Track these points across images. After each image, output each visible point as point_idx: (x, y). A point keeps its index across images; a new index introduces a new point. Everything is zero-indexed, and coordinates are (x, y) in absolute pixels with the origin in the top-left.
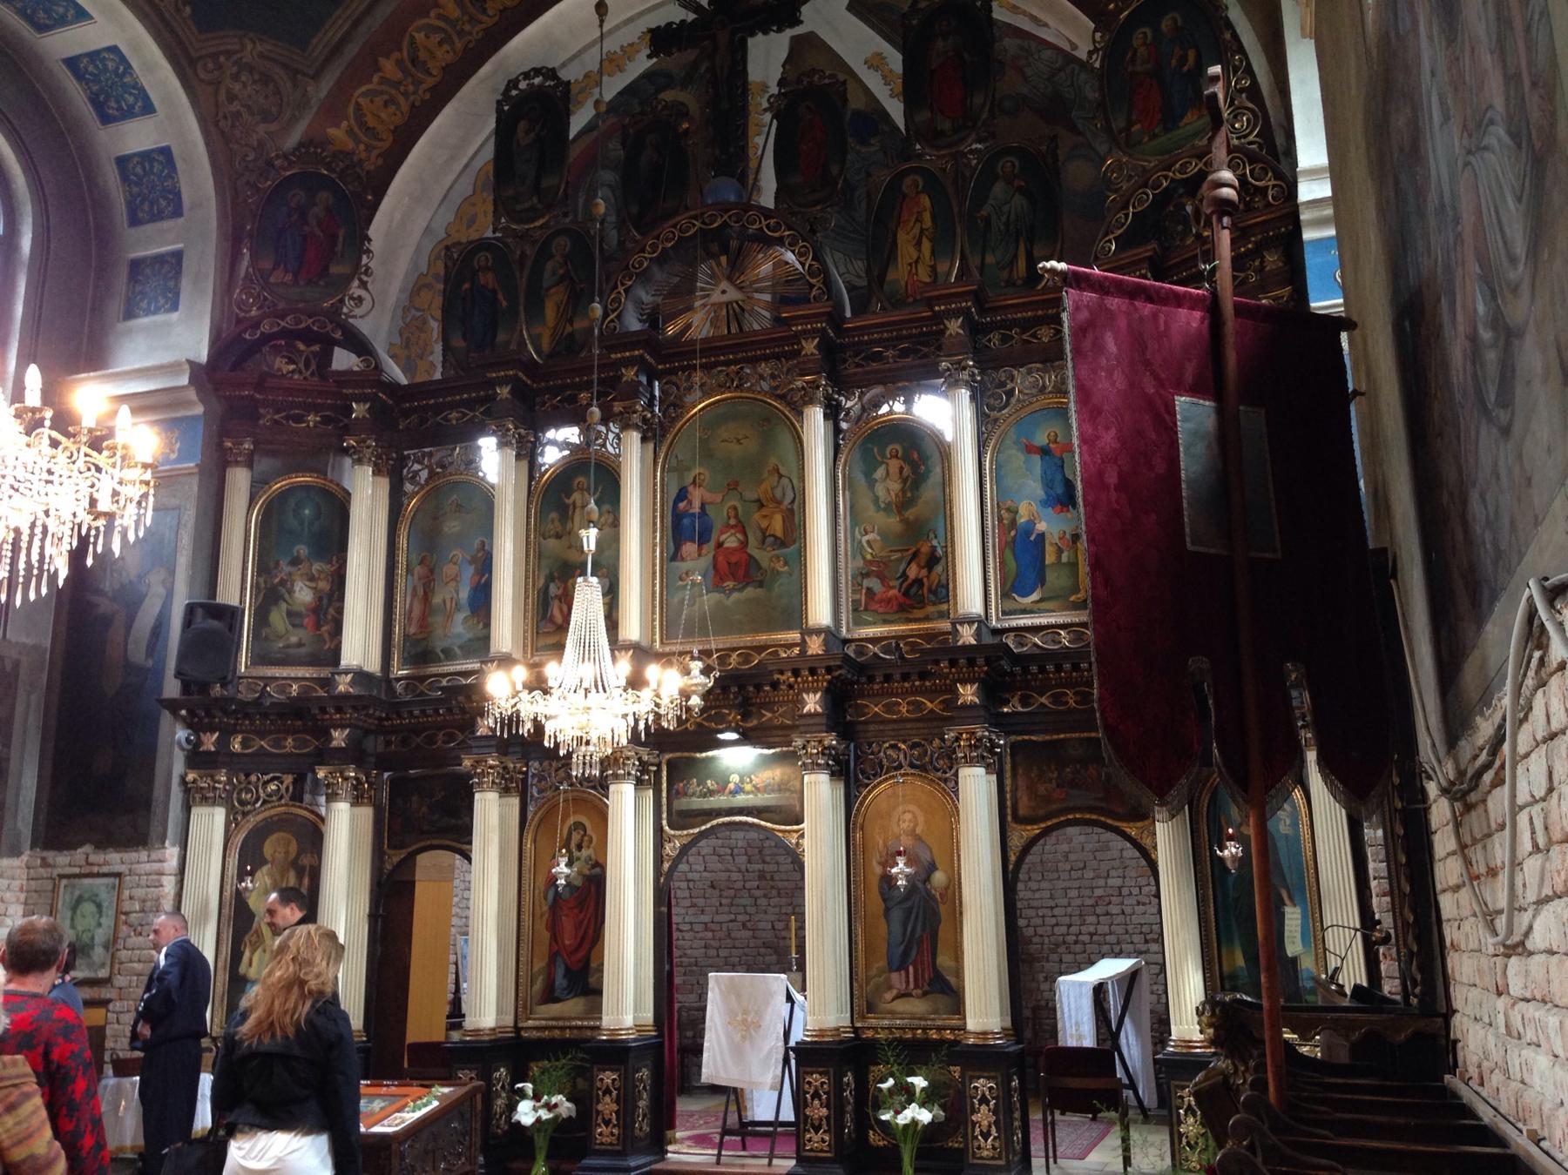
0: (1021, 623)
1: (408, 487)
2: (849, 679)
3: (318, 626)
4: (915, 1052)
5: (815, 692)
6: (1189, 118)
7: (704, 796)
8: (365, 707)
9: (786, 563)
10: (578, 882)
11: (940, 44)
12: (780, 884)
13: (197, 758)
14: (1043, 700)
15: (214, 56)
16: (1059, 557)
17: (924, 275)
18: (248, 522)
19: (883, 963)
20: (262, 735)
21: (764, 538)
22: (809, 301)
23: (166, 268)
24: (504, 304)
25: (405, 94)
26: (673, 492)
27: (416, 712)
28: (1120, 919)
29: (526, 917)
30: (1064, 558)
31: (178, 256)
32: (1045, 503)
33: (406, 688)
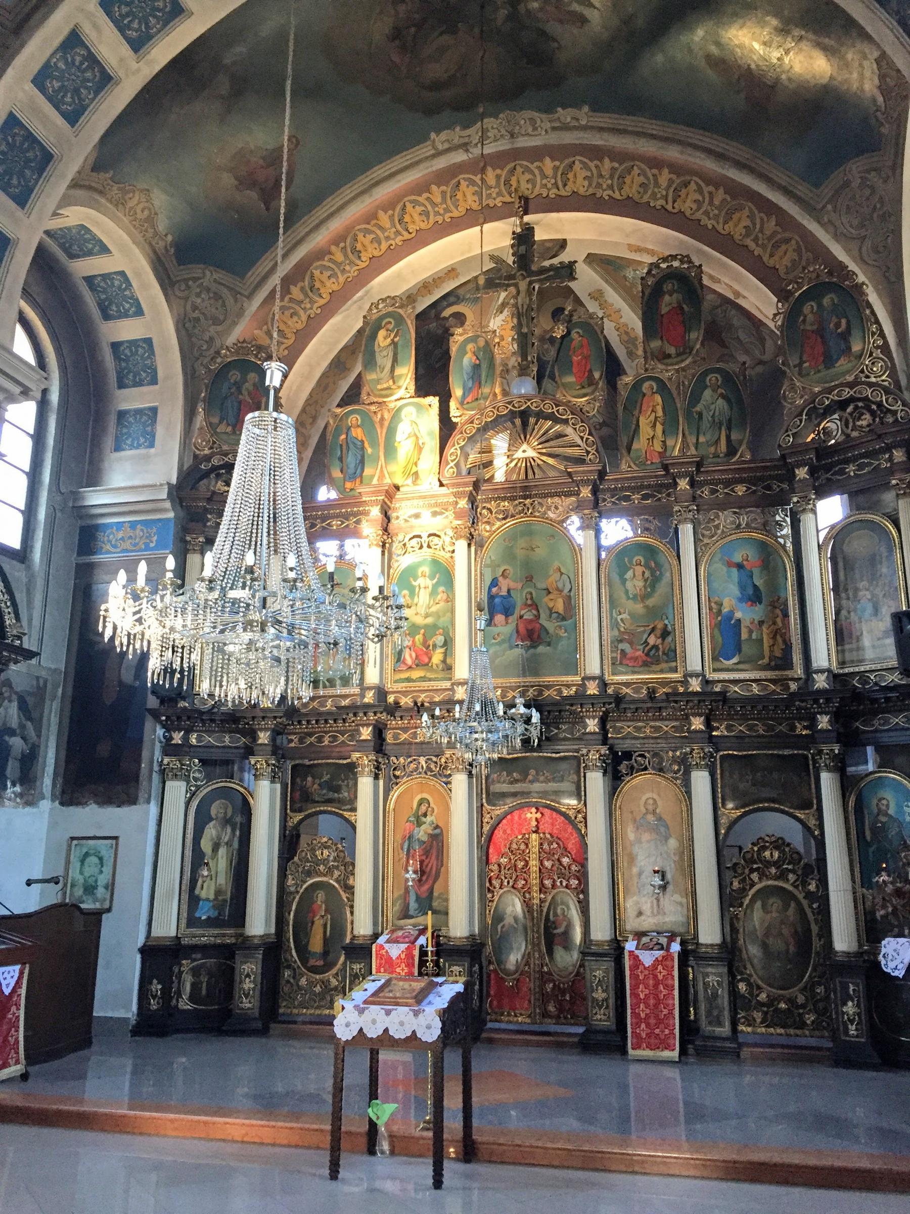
6: (842, 361)
11: (667, 298)
13: (169, 749)
15: (186, 281)
16: (750, 635)
17: (658, 447)
20: (209, 732)
23: (145, 418)
25: (304, 309)
26: (488, 581)
30: (754, 636)
31: (154, 410)
32: (741, 600)
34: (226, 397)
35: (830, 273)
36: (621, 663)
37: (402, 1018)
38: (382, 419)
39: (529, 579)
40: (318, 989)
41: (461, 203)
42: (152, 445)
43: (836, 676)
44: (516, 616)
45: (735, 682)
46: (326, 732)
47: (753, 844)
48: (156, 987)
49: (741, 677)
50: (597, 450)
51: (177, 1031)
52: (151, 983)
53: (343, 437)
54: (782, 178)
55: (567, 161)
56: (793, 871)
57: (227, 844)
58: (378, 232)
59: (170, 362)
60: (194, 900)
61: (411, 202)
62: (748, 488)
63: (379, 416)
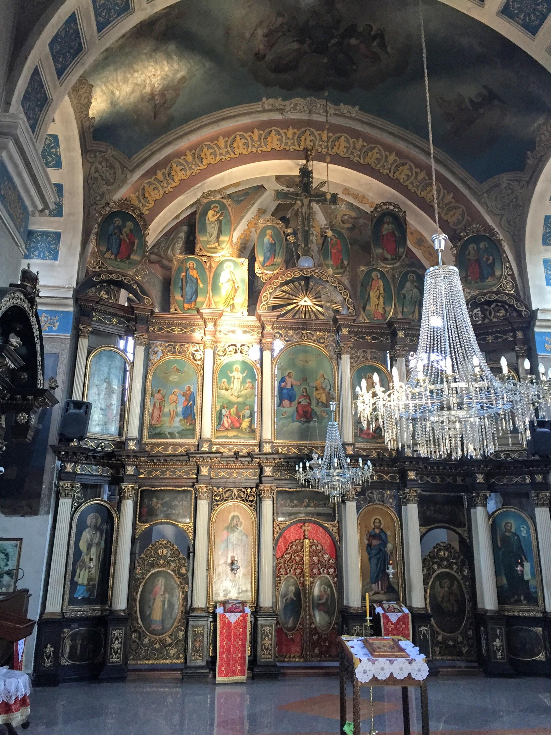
6: (489, 279)
9: (327, 414)
11: (386, 226)
15: (95, 151)
17: (381, 311)
21: (318, 402)
25: (163, 187)
31: (58, 236)
34: (111, 235)
35: (485, 231)
36: (360, 436)
37: (401, 665)
38: (210, 267)
39: (305, 380)
40: (157, 646)
41: (269, 143)
42: (55, 258)
44: (296, 402)
46: (168, 469)
47: (434, 548)
48: (49, 649)
50: (354, 307)
51: (65, 681)
52: (46, 647)
53: (184, 274)
54: (463, 173)
55: (337, 135)
56: (456, 564)
58: (216, 149)
59: (75, 203)
60: (74, 585)
61: (240, 135)
63: (208, 264)
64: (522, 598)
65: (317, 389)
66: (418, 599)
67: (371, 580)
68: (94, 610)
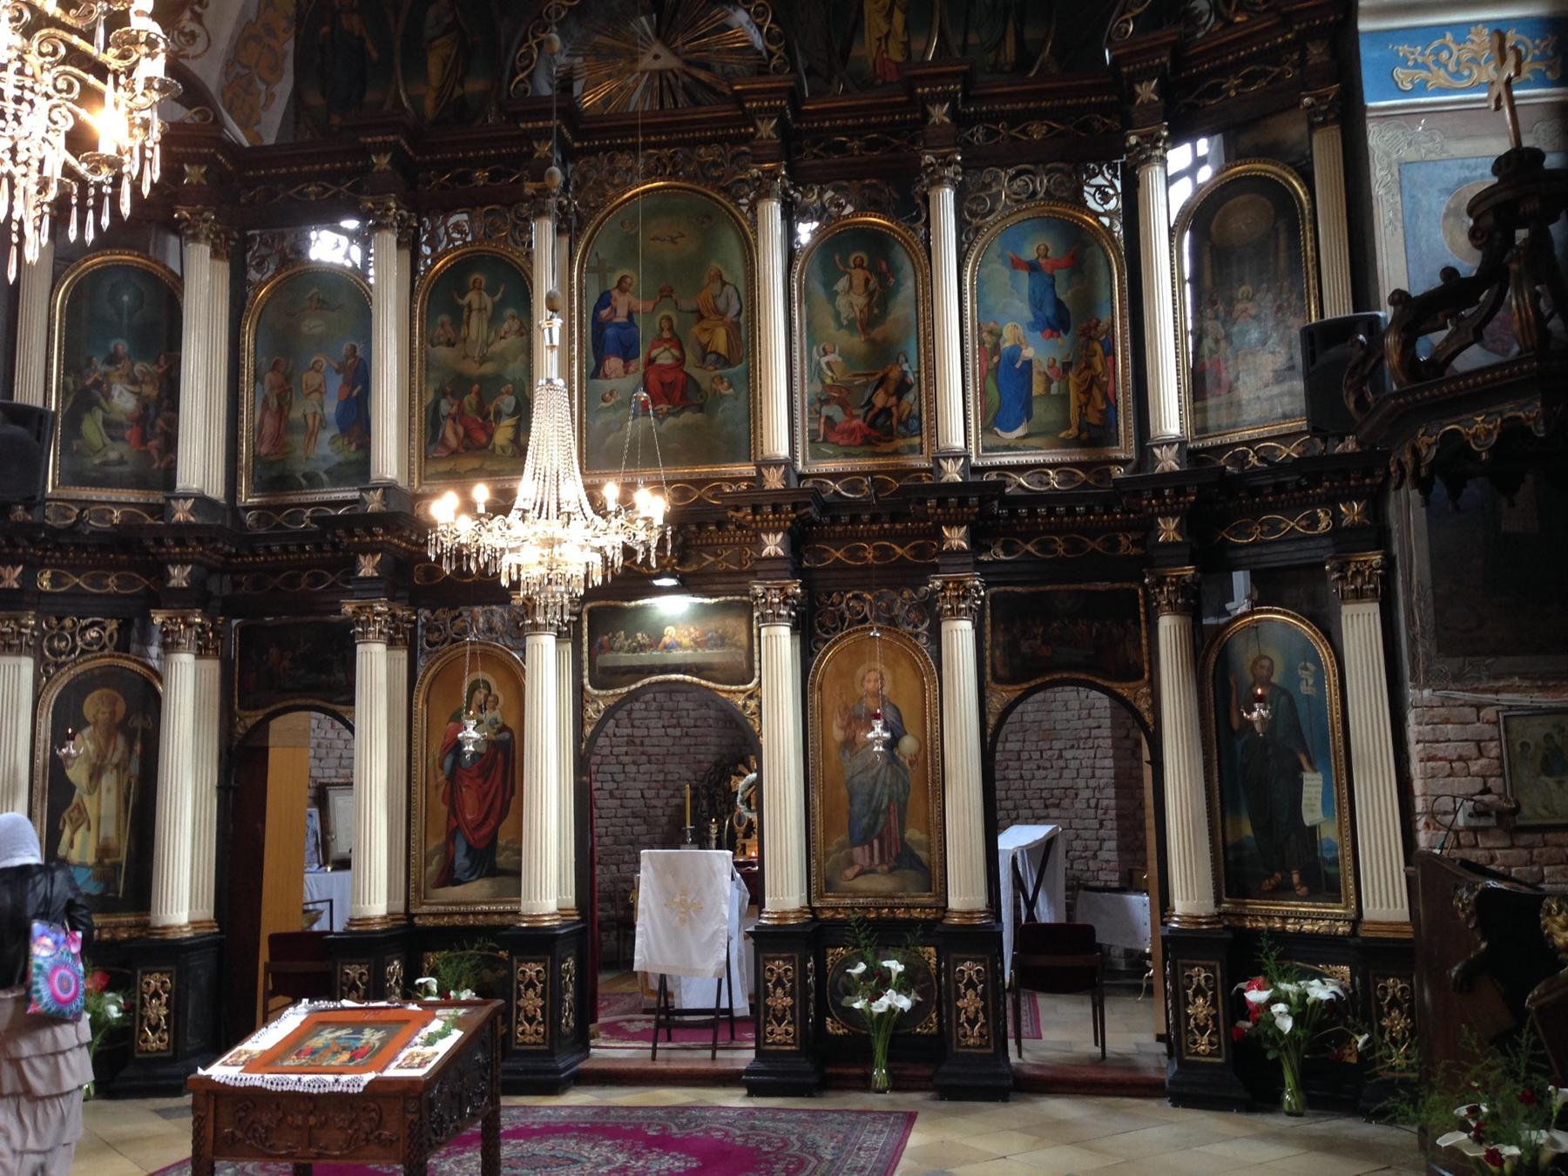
0: (1006, 460)
1: (254, 275)
2: (810, 515)
3: (144, 440)
4: (887, 932)
5: (776, 533)
7: (634, 650)
8: (212, 540)
9: (731, 385)
10: (483, 749)
12: (651, 750)
14: (1029, 547)
16: (1048, 389)
17: (896, 55)
18: (51, 308)
19: (843, 838)
22: (767, 73)
24: (375, 55)
27: (276, 548)
28: (1018, 784)
29: (419, 791)
30: (1054, 389)
32: (1033, 326)
33: (258, 520)
36: (825, 441)
43: (1192, 454)
45: (1020, 469)
49: (1032, 457)
57: (117, 766)
62: (1051, 129)
64: (1296, 878)
65: (701, 317)
66: (1385, 898)
67: (851, 836)
68: (117, 926)
